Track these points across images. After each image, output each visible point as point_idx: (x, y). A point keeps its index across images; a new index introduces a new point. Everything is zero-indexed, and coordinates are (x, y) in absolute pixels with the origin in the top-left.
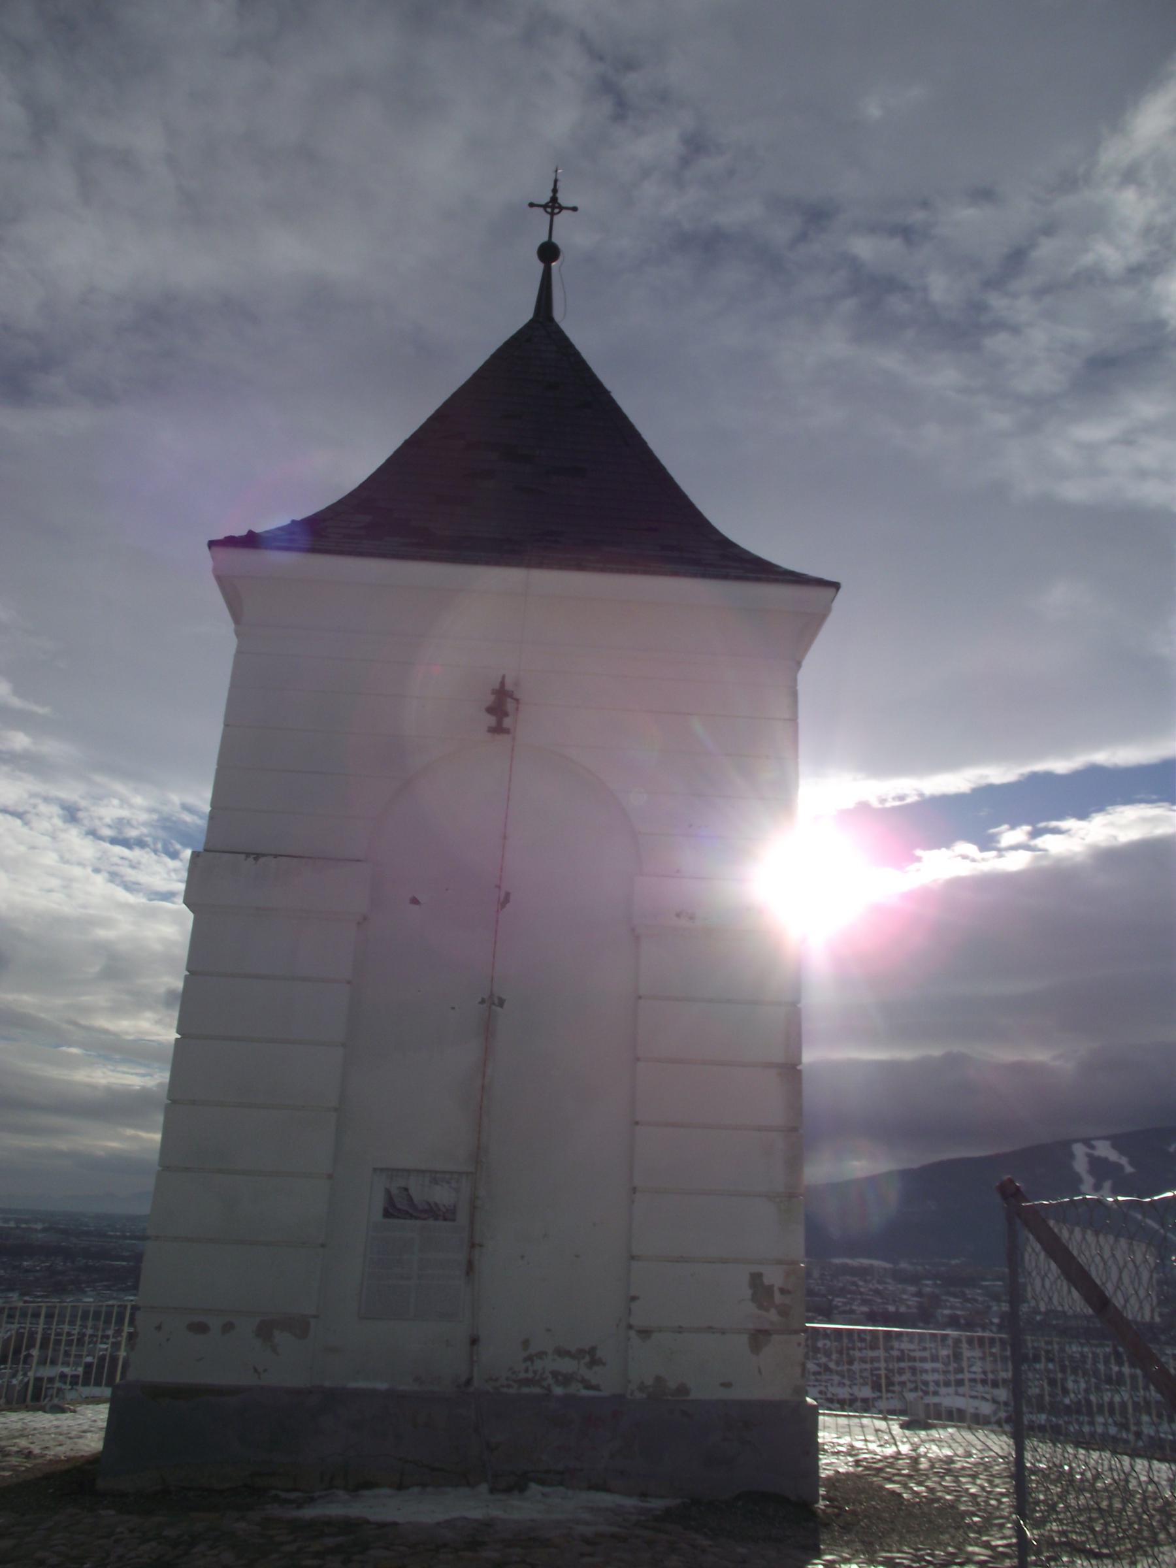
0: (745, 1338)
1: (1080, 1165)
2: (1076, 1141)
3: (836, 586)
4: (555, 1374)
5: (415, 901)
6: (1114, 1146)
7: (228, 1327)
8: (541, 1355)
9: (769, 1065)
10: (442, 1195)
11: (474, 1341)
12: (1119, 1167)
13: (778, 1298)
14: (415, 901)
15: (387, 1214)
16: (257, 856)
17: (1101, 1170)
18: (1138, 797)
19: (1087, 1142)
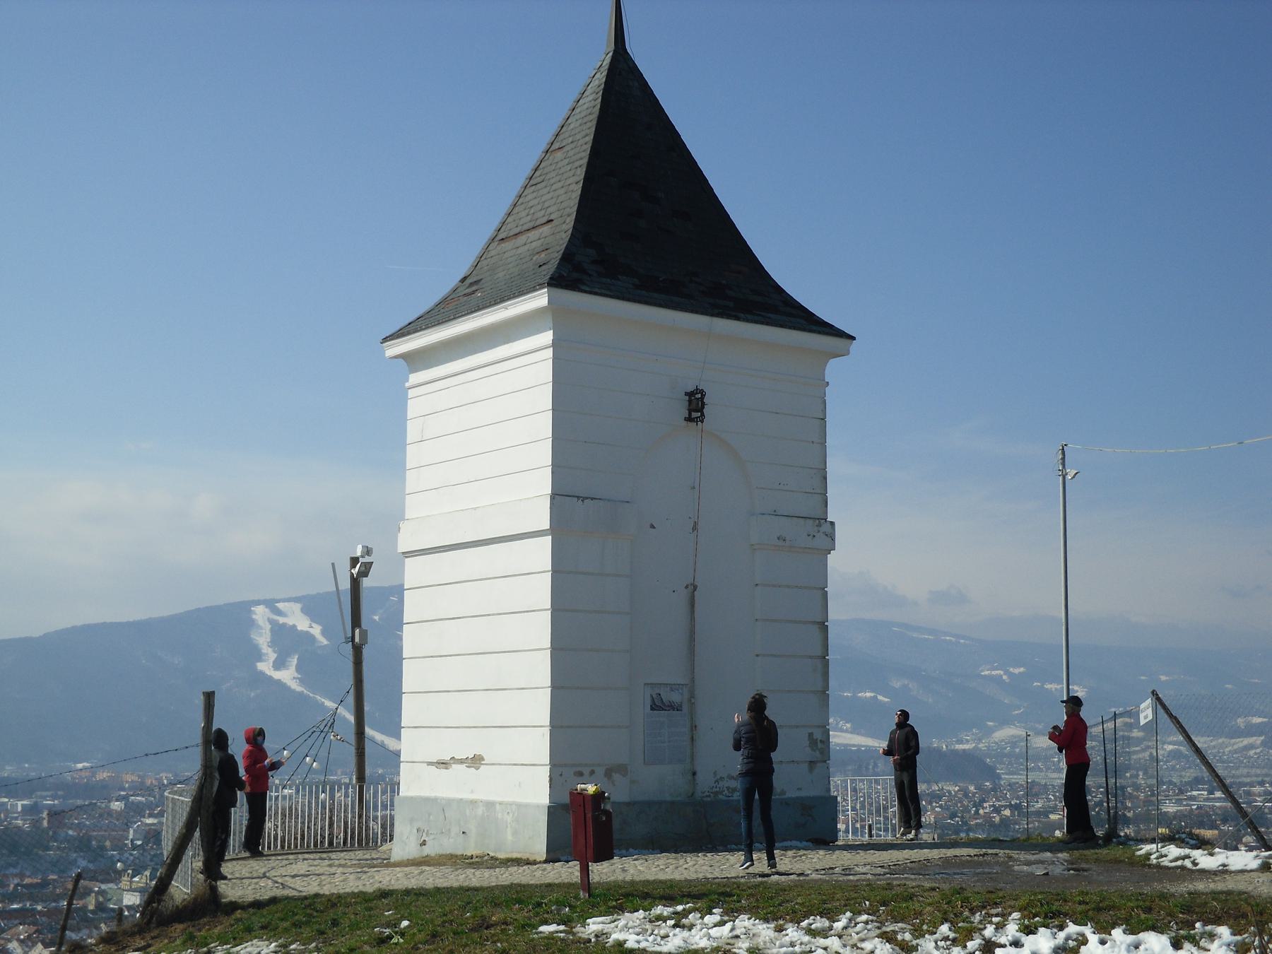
0: (806, 766)
1: (263, 639)
2: (258, 603)
3: (853, 338)
4: (728, 788)
5: (652, 526)
6: (306, 611)
7: (592, 772)
8: (722, 778)
9: (814, 623)
10: (675, 697)
11: (694, 774)
12: (309, 637)
13: (820, 745)
14: (652, 526)
15: (652, 709)
16: (584, 499)
17: (286, 639)
18: (584, 288)
19: (270, 604)
